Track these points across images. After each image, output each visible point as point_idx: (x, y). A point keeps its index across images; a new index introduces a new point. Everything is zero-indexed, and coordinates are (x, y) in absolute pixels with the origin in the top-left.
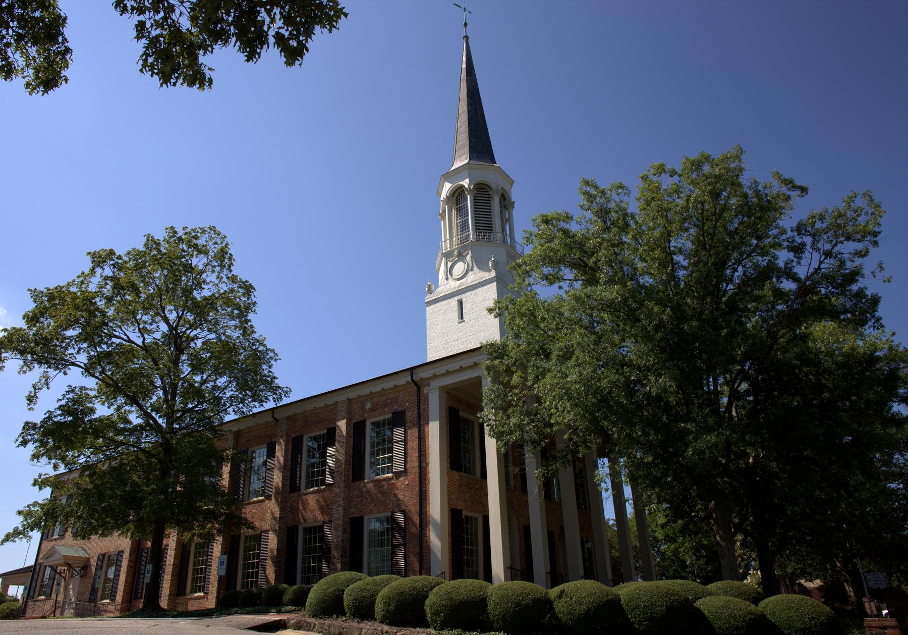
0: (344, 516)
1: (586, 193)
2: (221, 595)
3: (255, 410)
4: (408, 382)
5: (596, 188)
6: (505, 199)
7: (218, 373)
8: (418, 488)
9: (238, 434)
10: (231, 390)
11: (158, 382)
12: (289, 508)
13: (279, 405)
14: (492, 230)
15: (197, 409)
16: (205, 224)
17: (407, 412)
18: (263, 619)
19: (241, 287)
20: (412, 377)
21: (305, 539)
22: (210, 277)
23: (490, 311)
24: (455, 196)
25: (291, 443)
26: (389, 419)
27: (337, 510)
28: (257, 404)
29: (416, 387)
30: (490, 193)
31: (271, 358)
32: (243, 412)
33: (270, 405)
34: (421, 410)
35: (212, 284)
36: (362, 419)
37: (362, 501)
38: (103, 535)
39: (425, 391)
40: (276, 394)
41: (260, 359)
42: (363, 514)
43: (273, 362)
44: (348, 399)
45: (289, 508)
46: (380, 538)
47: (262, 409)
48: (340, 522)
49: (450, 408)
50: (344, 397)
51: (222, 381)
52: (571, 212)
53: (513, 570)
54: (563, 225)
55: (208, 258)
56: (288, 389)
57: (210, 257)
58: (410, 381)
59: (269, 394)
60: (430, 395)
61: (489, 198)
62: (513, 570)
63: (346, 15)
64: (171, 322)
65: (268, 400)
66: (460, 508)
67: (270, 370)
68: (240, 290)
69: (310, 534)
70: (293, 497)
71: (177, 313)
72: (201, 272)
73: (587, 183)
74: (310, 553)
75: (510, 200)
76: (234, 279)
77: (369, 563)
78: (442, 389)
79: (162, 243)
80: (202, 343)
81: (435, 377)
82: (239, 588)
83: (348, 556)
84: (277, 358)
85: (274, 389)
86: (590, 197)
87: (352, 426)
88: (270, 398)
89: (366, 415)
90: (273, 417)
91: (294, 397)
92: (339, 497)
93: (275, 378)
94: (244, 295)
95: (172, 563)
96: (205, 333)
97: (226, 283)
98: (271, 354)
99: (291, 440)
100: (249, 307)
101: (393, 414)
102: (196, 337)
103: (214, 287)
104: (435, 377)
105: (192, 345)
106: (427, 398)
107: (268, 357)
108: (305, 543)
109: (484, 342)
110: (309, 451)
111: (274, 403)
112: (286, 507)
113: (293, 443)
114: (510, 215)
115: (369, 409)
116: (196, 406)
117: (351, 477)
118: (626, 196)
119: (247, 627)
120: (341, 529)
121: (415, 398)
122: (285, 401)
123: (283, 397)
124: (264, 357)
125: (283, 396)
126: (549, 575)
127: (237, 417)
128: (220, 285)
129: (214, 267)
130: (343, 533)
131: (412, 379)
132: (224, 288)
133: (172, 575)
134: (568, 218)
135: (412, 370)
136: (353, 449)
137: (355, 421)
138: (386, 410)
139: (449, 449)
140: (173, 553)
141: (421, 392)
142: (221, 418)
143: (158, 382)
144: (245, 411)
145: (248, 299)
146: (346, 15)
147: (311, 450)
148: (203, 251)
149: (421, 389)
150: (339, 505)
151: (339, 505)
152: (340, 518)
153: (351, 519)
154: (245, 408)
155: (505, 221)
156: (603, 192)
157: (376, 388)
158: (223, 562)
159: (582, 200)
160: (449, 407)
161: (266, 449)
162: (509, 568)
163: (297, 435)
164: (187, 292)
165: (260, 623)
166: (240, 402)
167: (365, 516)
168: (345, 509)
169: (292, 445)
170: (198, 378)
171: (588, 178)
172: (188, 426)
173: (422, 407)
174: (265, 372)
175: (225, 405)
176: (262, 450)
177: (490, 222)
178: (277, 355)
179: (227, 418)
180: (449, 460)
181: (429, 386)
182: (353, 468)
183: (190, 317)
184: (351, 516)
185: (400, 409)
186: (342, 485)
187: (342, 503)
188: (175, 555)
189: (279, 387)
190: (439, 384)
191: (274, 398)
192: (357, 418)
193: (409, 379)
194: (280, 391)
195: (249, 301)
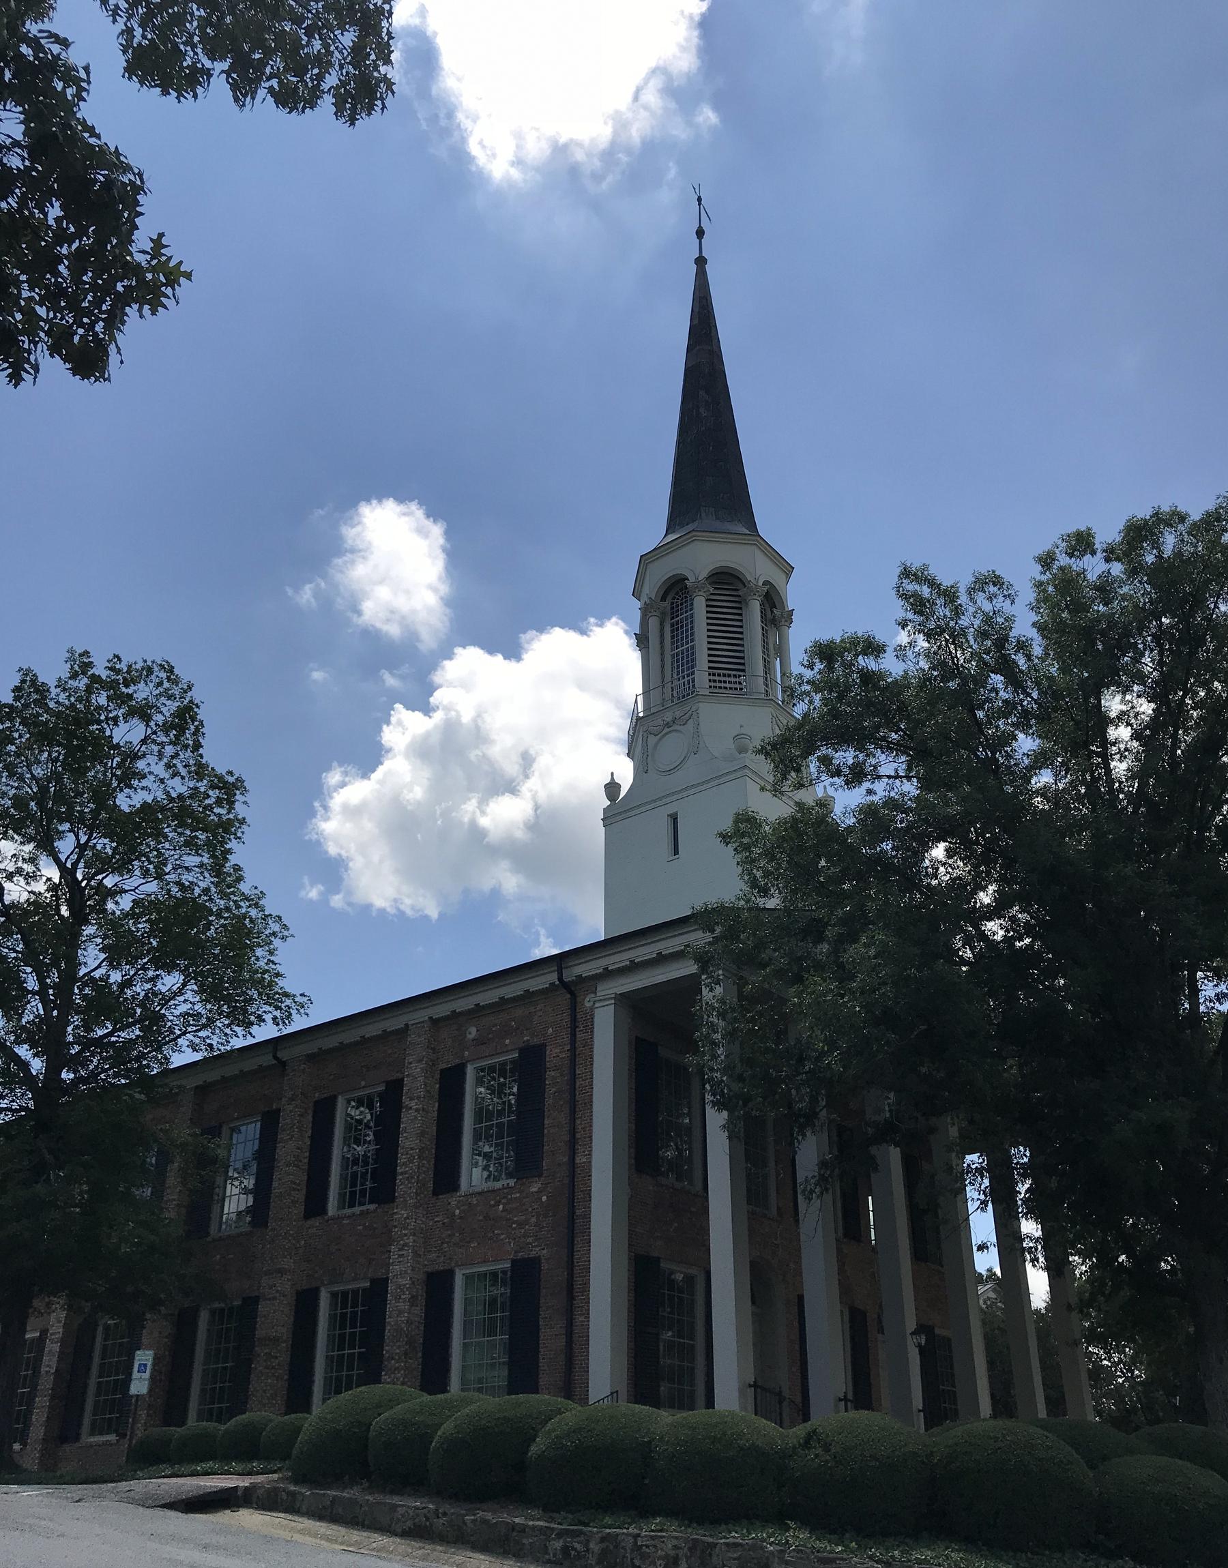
1: (904, 596)
3: (238, 1043)
4: (552, 984)
5: (933, 584)
6: (773, 606)
7: (164, 962)
9: (203, 1090)
10: (185, 1001)
11: (32, 983)
13: (285, 1032)
14: (743, 671)
15: (113, 1039)
16: (155, 655)
18: (199, 1487)
19: (213, 787)
22: (151, 765)
23: (725, 838)
24: (669, 599)
25: (310, 1112)
26: (513, 1062)
27: (400, 1256)
28: (239, 1030)
29: (569, 996)
30: (740, 593)
31: (274, 934)
32: (211, 1045)
33: (265, 1032)
35: (152, 778)
36: (458, 1061)
39: (588, 1004)
40: (277, 1008)
41: (249, 934)
43: (277, 942)
44: (431, 1018)
47: (250, 1041)
48: (406, 1281)
51: (170, 981)
52: (880, 637)
53: (759, 1390)
54: (863, 662)
55: (147, 726)
56: (305, 999)
57: (152, 724)
58: (557, 983)
59: (267, 1008)
60: (597, 1012)
61: (740, 604)
62: (759, 1390)
63: (188, 276)
64: (63, 857)
65: (264, 1021)
66: (656, 1254)
67: (272, 958)
68: (211, 793)
69: (344, 1306)
71: (78, 839)
72: (135, 756)
73: (906, 573)
74: (341, 1348)
75: (783, 605)
76: (200, 771)
78: (623, 1000)
79: (54, 691)
80: (134, 901)
81: (607, 974)
83: (420, 1355)
84: (286, 933)
85: (275, 998)
86: (919, 605)
87: (438, 1076)
88: (268, 1017)
90: (275, 1057)
91: (318, 1015)
92: (406, 1229)
93: (278, 975)
94: (219, 802)
95: (53, 1371)
96: (135, 881)
97: (183, 778)
98: (275, 927)
100: (228, 827)
102: (116, 892)
103: (155, 785)
104: (607, 974)
105: (110, 906)
107: (267, 932)
109: (699, 905)
110: (348, 1128)
111: (276, 1028)
114: (783, 639)
116: (111, 1034)
117: (431, 1185)
118: (1008, 602)
119: (157, 1503)
120: (407, 1296)
121: (567, 1018)
122: (299, 1023)
123: (295, 1016)
124: (258, 933)
125: (294, 1012)
126: (922, 1414)
127: (198, 1057)
128: (170, 783)
129: (162, 744)
130: (412, 1305)
131: (560, 979)
132: (178, 787)
133: (53, 1398)
134: (873, 648)
136: (438, 1126)
137: (444, 1066)
138: (507, 1042)
140: (56, 1347)
142: (166, 1058)
143: (32, 983)
144: (214, 1043)
145: (229, 813)
146: (188, 276)
147: (355, 1132)
148: (143, 712)
149: (579, 999)
150: (406, 1245)
152: (406, 1272)
154: (215, 1037)
155: (772, 652)
156: (950, 596)
158: (145, 1365)
159: (899, 610)
160: (637, 1037)
161: (259, 1124)
162: (750, 1386)
164: (102, 796)
165: (195, 1493)
166: (204, 1027)
170: (116, 977)
171: (915, 564)
172: (94, 1075)
173: (580, 1036)
174: (262, 963)
175: (171, 1031)
177: (711, 659)
178: (285, 927)
179: (177, 1060)
180: (632, 1150)
182: (435, 1165)
183: (104, 844)
185: (536, 1041)
188: (61, 1353)
189: (286, 995)
191: (275, 1019)
192: (446, 1063)
193: (554, 978)
194: (288, 1002)
195: (231, 816)
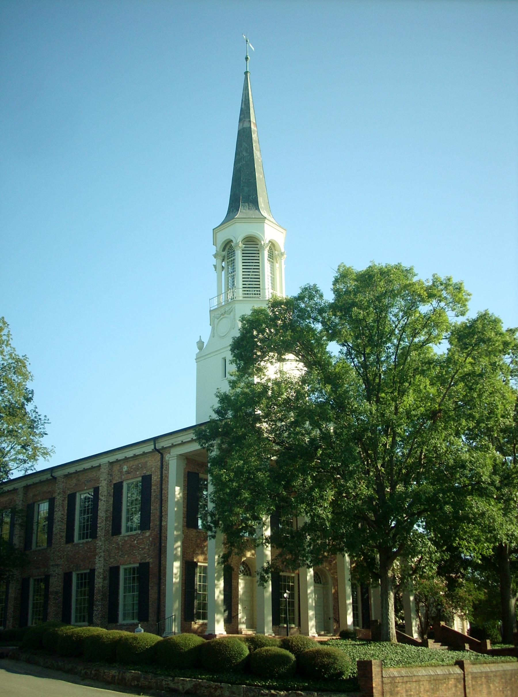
0: (104, 566)
2: (423, 627)
8: (158, 545)
12: (65, 557)
17: (153, 476)
20: (155, 446)
21: (77, 584)
34: (163, 475)
36: (120, 480)
37: (118, 553)
38: (408, 272)
39: (167, 459)
42: (119, 564)
45: (65, 557)
46: (202, 575)
49: (189, 472)
50: (104, 460)
70: (68, 547)
77: (124, 605)
81: (173, 446)
82: (29, 624)
87: (113, 486)
89: (123, 477)
99: (67, 496)
101: (143, 477)
104: (173, 446)
106: (168, 465)
108: (78, 587)
112: (64, 556)
113: (68, 499)
115: (126, 471)
135: (155, 440)
137: (115, 482)
138: (138, 473)
139: (185, 509)
141: (164, 459)
149: (164, 456)
151: (101, 556)
153: (111, 568)
157: (130, 454)
163: (71, 493)
167: (121, 566)
168: (105, 560)
169: (68, 501)
173: (164, 472)
176: (46, 503)
181: (169, 453)
184: (111, 566)
185: (148, 473)
186: (103, 539)
187: (102, 554)
190: (176, 453)
192: (116, 480)
